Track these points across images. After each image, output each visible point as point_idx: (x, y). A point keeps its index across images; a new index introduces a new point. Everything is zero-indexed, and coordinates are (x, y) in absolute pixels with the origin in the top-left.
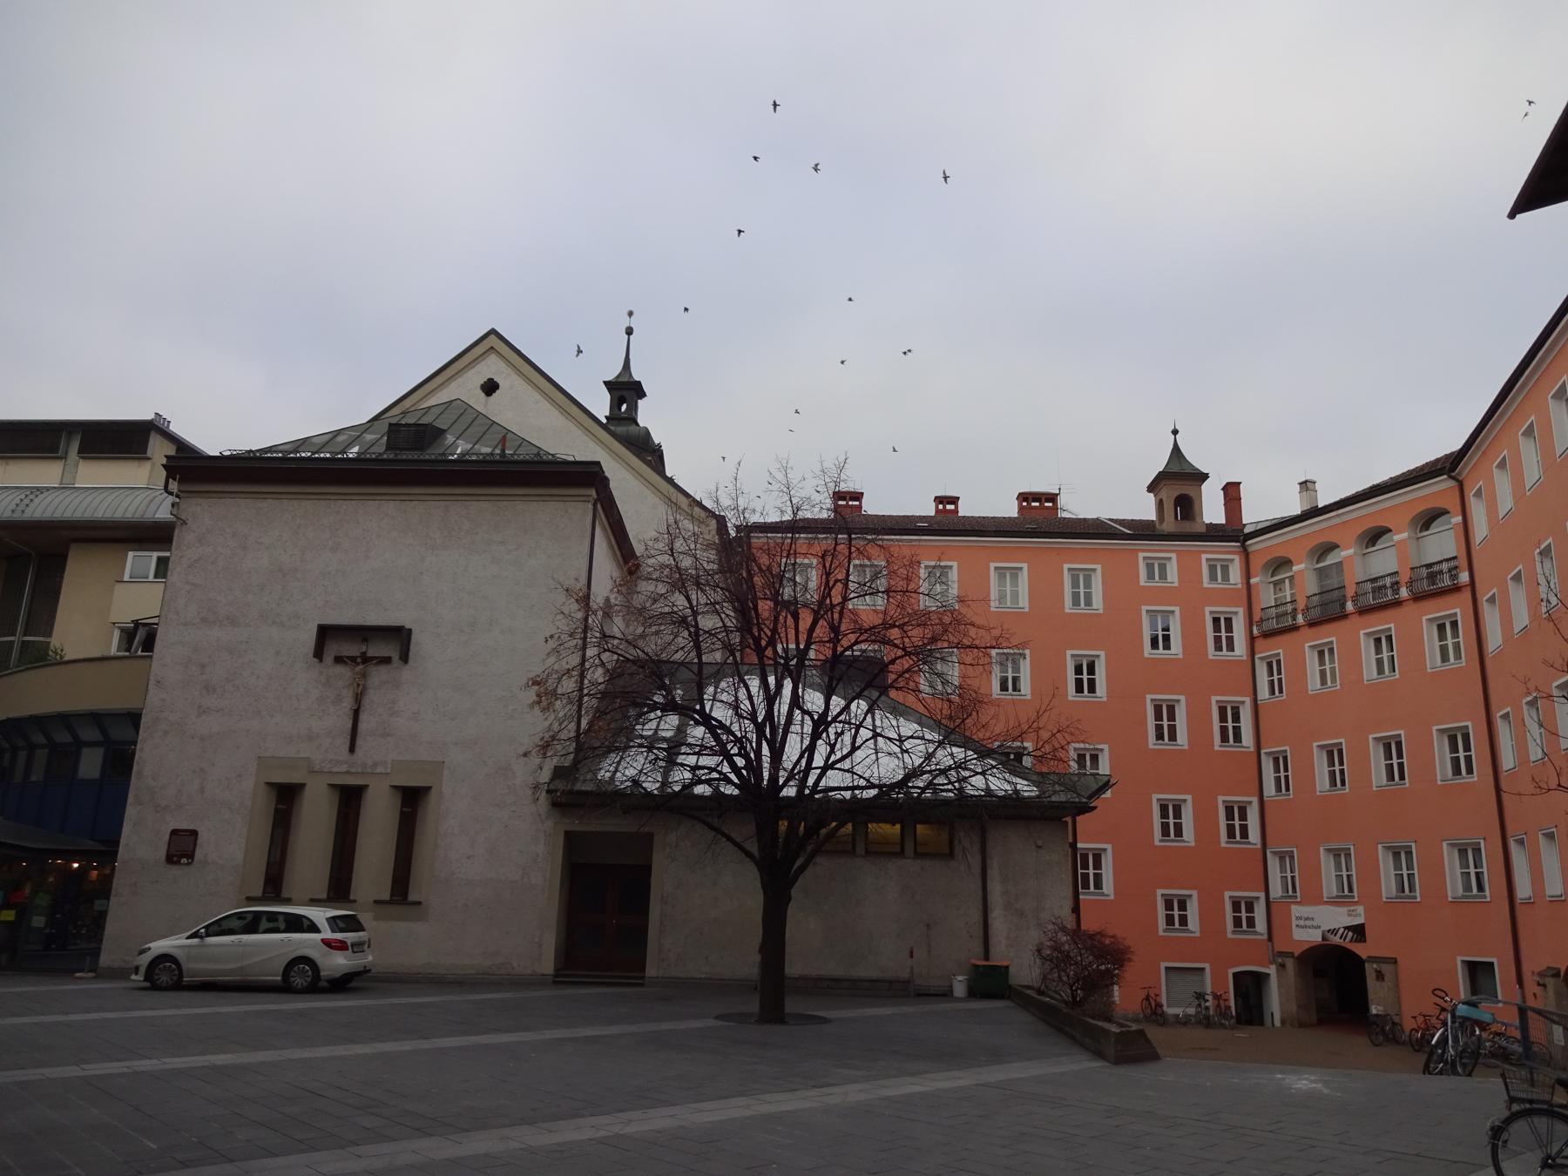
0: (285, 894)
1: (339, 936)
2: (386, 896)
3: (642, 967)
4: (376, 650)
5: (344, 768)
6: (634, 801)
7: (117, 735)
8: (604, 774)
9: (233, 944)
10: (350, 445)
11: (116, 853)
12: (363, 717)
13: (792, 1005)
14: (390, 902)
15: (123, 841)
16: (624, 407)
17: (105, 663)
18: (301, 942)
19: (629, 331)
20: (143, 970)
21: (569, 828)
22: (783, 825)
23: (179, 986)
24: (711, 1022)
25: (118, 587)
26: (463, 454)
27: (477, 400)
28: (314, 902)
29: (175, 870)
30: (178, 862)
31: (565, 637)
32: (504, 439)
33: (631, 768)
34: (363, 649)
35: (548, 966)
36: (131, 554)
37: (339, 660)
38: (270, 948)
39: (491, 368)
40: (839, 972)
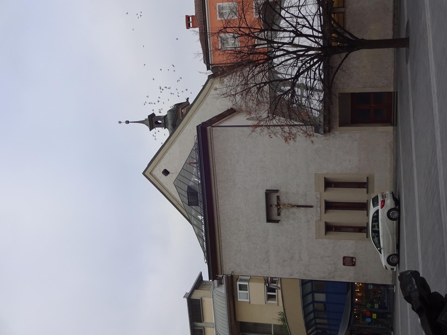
0: (365, 225)
1: (380, 203)
2: (365, 190)
3: (390, 93)
4: (275, 202)
5: (319, 209)
6: (326, 102)
7: (310, 287)
8: (316, 114)
9: (383, 238)
10: (198, 219)
11: (352, 283)
12: (300, 204)
13: (403, 36)
14: (367, 188)
15: (348, 281)
16: (160, 122)
17: (284, 296)
18: (382, 216)
19: (127, 122)
20: (392, 267)
21: (338, 125)
22: (334, 44)
23: (398, 255)
24: (409, 65)
25: (252, 303)
26: (198, 178)
27: (172, 177)
28: (368, 215)
29: (358, 263)
30: (355, 262)
31: (270, 131)
32: (190, 163)
33: (316, 103)
34: (274, 206)
35: (390, 129)
36: (239, 300)
37: (279, 214)
38: (384, 226)
39: (158, 173)
40: (391, 15)
